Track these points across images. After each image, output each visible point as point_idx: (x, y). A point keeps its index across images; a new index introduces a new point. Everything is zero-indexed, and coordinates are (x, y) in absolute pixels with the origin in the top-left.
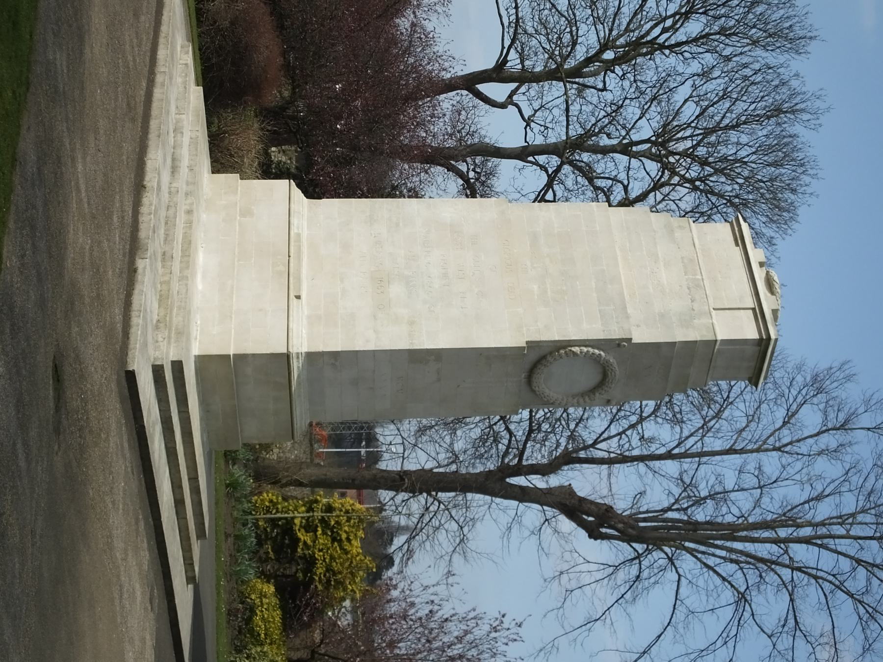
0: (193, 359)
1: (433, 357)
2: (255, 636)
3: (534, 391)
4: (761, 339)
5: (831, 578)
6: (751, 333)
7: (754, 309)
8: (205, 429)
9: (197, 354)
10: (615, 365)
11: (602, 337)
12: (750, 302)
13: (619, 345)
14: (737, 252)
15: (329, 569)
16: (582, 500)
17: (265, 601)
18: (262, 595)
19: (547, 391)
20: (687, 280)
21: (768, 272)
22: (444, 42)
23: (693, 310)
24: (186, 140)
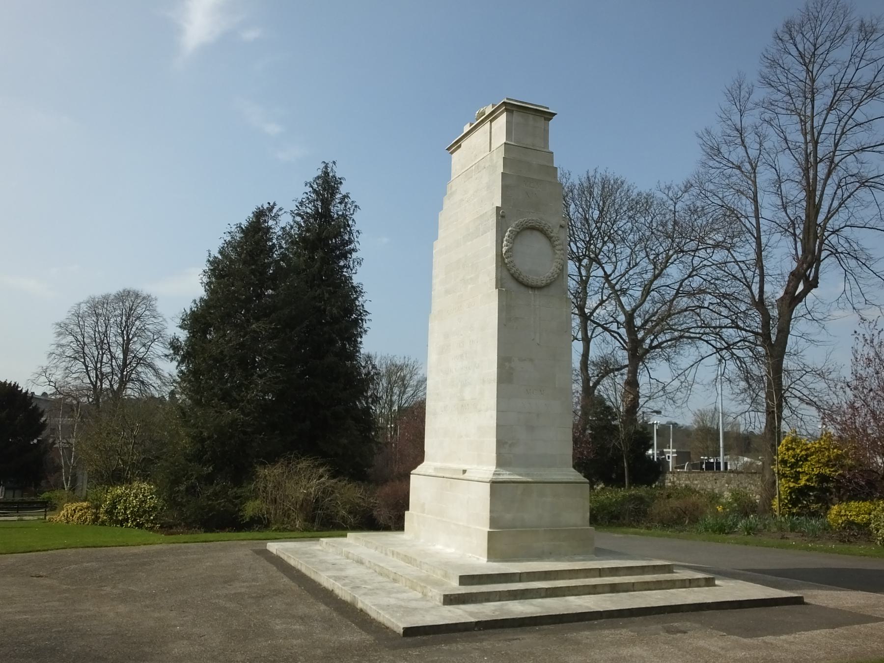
0: (490, 564)
2: (868, 524)
3: (548, 285)
4: (506, 110)
5: (842, 124)
8: (540, 556)
9: (486, 559)
13: (503, 217)
14: (465, 144)
15: (826, 465)
16: (786, 293)
17: (843, 513)
18: (839, 514)
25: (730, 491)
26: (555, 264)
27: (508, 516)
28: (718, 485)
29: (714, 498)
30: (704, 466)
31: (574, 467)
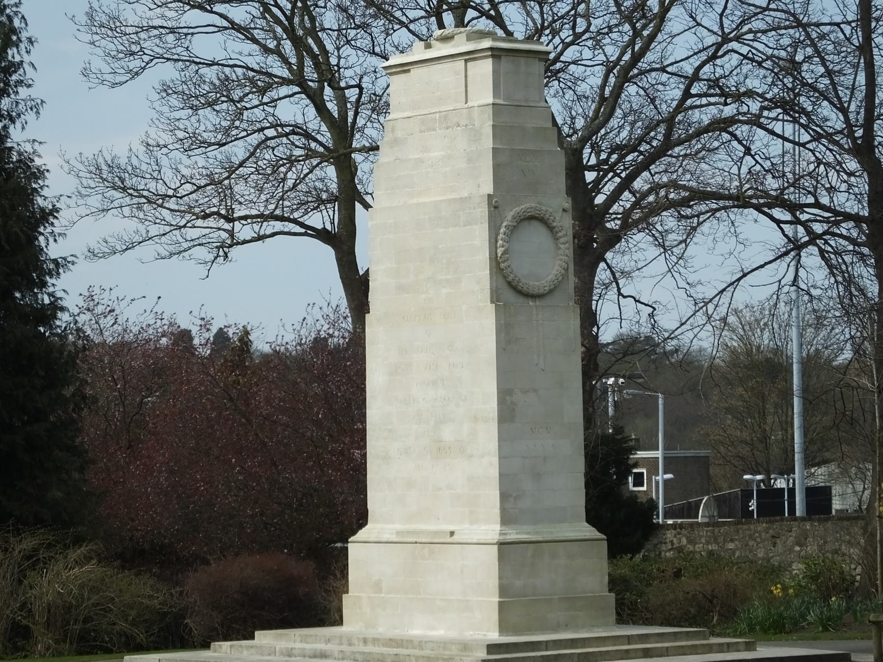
1: (508, 398)
3: (551, 291)
4: (493, 56)
6: (485, 68)
7: (466, 61)
10: (518, 209)
11: (486, 226)
12: (460, 64)
13: (496, 207)
14: (415, 72)
19: (550, 277)
20: (440, 129)
21: (437, 40)
22: (282, 332)
23: (466, 126)
24: (299, 645)
25: (805, 559)
26: (558, 262)
27: (519, 583)
28: (780, 547)
29: (773, 572)
30: (753, 505)
31: (588, 521)
